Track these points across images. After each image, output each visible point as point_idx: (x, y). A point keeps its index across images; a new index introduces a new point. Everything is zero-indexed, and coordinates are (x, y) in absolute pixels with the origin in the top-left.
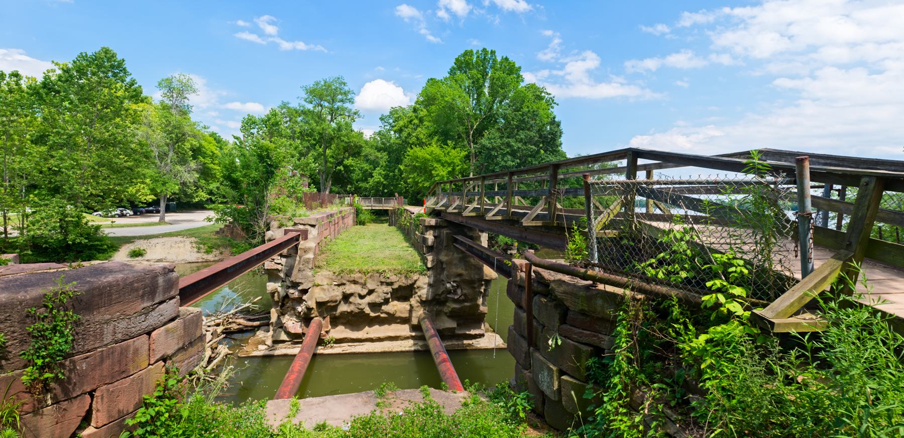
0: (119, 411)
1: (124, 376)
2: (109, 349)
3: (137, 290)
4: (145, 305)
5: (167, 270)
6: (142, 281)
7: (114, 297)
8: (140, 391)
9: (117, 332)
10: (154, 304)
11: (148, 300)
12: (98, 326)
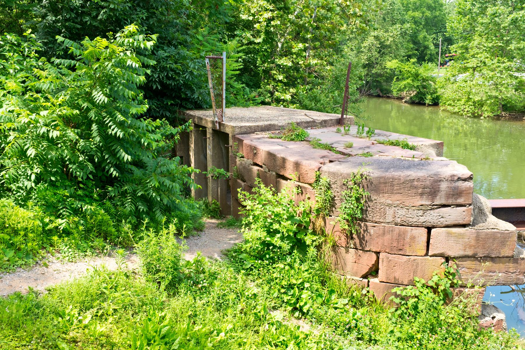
0: (395, 278)
1: (400, 253)
2: (390, 227)
3: (416, 187)
4: (424, 203)
5: (456, 178)
6: (422, 182)
7: (395, 188)
8: (415, 273)
9: (397, 216)
10: (433, 205)
11: (427, 199)
12: (382, 206)
